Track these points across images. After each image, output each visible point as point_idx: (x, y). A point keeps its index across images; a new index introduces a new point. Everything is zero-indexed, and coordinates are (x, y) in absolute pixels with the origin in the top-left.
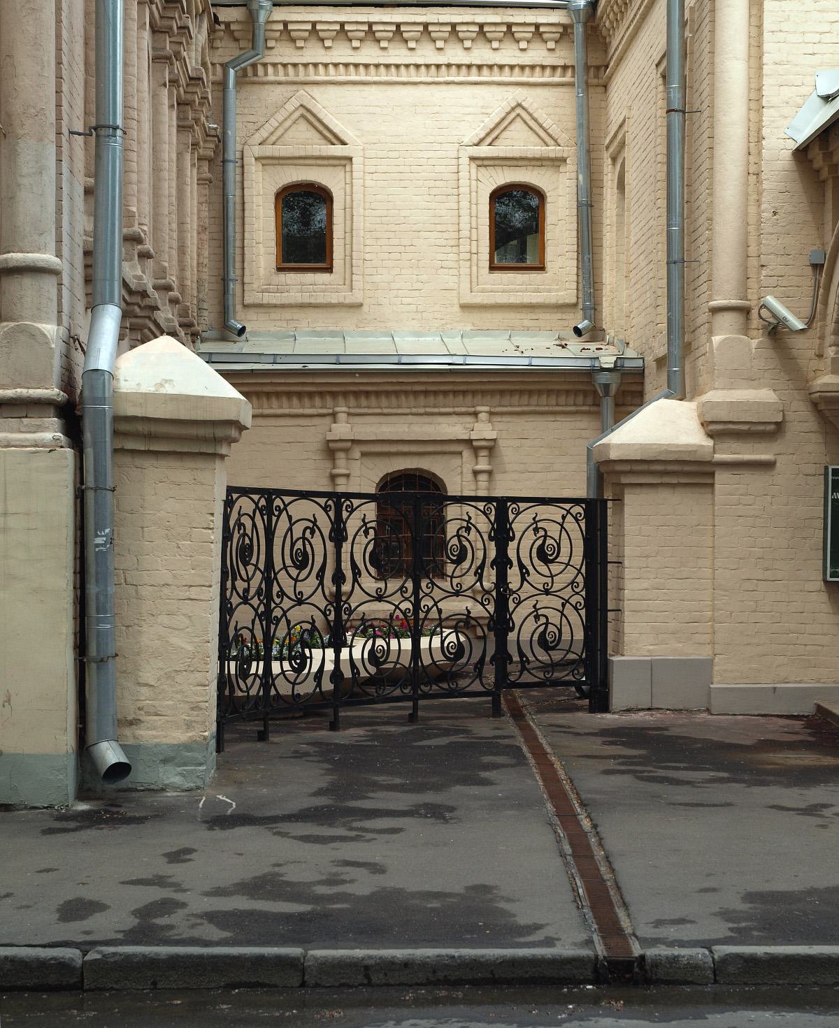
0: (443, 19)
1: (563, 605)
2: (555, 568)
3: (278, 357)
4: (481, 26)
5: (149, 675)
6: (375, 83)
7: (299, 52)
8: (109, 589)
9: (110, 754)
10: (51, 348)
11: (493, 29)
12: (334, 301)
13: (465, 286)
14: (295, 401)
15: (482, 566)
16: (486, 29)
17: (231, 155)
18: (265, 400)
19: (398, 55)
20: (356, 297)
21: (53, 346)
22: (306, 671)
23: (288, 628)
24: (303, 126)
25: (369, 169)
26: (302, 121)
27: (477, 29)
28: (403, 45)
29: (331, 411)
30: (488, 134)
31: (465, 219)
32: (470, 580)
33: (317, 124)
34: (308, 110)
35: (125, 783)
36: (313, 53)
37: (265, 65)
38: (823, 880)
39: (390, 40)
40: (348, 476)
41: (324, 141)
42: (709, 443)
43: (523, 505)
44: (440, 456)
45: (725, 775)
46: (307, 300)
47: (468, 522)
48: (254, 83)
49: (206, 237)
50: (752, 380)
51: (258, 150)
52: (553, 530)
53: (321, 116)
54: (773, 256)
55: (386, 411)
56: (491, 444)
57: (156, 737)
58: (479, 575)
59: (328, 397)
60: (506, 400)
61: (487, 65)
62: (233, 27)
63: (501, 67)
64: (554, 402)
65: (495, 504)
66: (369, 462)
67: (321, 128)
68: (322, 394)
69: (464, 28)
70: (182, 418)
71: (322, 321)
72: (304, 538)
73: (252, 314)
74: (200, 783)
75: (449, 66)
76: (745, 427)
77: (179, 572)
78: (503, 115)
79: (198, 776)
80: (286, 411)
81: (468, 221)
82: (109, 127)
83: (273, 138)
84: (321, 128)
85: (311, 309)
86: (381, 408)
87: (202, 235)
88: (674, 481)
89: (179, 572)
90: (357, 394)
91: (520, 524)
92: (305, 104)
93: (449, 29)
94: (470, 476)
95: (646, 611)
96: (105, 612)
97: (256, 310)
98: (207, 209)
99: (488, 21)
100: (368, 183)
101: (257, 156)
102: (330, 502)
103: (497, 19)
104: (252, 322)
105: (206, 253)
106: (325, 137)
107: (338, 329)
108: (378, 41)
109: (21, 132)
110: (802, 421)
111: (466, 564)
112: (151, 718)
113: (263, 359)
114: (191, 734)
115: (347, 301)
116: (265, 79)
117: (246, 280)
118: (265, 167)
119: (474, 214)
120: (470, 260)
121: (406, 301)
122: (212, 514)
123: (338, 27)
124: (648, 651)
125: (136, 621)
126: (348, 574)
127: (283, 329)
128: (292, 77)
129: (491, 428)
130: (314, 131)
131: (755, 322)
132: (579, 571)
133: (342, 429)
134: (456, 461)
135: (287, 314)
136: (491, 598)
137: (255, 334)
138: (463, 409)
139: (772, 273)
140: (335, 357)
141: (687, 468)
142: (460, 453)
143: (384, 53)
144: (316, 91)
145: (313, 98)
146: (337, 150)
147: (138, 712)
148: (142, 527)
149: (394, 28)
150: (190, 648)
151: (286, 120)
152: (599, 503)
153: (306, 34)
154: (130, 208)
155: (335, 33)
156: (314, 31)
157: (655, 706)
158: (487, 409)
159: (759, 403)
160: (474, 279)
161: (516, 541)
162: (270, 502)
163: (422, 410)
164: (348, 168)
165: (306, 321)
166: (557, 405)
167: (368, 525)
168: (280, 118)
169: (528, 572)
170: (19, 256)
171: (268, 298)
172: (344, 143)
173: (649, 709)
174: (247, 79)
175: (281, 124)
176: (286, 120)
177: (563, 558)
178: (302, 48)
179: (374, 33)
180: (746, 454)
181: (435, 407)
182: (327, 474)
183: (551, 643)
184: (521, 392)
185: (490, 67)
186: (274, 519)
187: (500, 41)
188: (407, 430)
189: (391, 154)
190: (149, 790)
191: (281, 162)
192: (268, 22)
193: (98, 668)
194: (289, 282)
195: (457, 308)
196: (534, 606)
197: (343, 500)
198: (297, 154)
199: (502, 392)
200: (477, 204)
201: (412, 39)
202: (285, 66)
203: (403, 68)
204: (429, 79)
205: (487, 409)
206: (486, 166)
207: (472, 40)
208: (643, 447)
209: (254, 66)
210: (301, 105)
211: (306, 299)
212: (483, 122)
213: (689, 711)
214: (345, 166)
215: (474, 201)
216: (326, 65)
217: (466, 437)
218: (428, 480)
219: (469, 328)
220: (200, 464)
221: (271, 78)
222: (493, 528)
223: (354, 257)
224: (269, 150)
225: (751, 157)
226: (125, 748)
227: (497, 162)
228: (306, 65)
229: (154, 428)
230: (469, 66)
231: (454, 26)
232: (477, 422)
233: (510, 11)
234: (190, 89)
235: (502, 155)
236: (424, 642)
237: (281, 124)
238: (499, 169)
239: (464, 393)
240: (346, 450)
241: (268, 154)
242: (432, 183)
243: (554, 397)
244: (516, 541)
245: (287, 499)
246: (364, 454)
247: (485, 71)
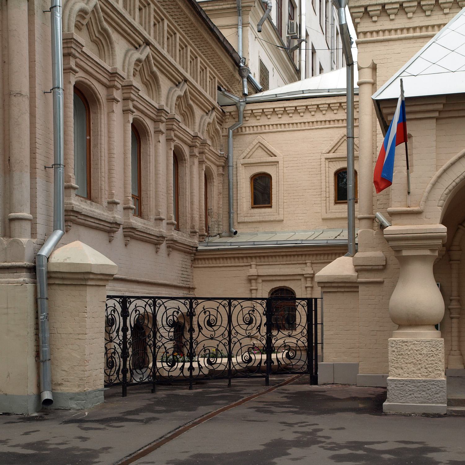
0: (313, 103)
1: (297, 341)
2: (215, 328)
3: (232, 243)
4: (329, 104)
5: (65, 367)
6: (288, 131)
7: (258, 121)
8: (46, 335)
9: (47, 395)
10: (24, 247)
11: (334, 105)
12: (272, 219)
13: (324, 210)
14: (236, 260)
15: (260, 326)
16: (331, 105)
17: (231, 164)
18: (203, 261)
19: (296, 119)
20: (281, 217)
21: (25, 246)
22: (175, 367)
23: (106, 350)
24: (260, 150)
25: (285, 166)
26: (259, 148)
27: (327, 106)
28: (298, 115)
29: (249, 264)
30: (332, 148)
31: (324, 183)
32: (255, 331)
33: (265, 149)
34: (262, 144)
35: (49, 407)
36: (264, 121)
37: (245, 127)
38: (464, 460)
39: (293, 113)
40: (257, 290)
41: (268, 156)
42: (356, 274)
43: (200, 301)
44: (293, 281)
45: (164, 408)
46: (261, 220)
47: (253, 308)
48: (241, 135)
49: (221, 196)
50: (373, 248)
51: (242, 161)
52: (213, 312)
53: (266, 146)
54: (382, 196)
55: (271, 263)
56: (312, 275)
57: (68, 390)
58: (259, 328)
59: (207, 261)
60: (318, 257)
61: (332, 120)
62: (232, 114)
63: (338, 120)
64: (323, 259)
65: (266, 301)
66: (264, 283)
67: (267, 150)
68: (246, 257)
69: (322, 106)
70: (78, 272)
71: (268, 228)
72: (111, 314)
73: (241, 226)
74: (83, 408)
75: (317, 122)
76: (370, 267)
77: (75, 329)
78: (339, 140)
79: (82, 405)
80: (233, 264)
81: (325, 184)
82: (58, 164)
83: (248, 156)
84: (267, 150)
85: (264, 223)
86: (269, 262)
87: (220, 196)
88: (343, 290)
89: (75, 329)
90: (260, 257)
91: (198, 310)
92: (260, 141)
93: (316, 107)
94: (304, 289)
95: (332, 344)
96: (45, 343)
97: (243, 224)
98: (221, 186)
99: (332, 102)
100: (285, 171)
101: (242, 163)
102: (187, 301)
103: (335, 101)
104: (240, 229)
105: (221, 203)
106: (269, 154)
107: (274, 230)
108: (299, 113)
109: (14, 169)
111: (253, 325)
112: (66, 383)
113: (226, 244)
114: (79, 389)
115: (277, 219)
116: (245, 133)
117: (239, 212)
118: (246, 167)
119: (327, 181)
120: (326, 200)
121: (300, 218)
122: (86, 307)
123: (272, 110)
124: (333, 360)
125: (61, 347)
126: (196, 329)
127: (253, 231)
128: (256, 131)
129: (311, 269)
130: (264, 152)
131: (376, 224)
132: (226, 329)
133: (253, 271)
134: (299, 282)
135: (254, 225)
136: (264, 338)
137: (242, 234)
138: (301, 262)
139: (381, 203)
140: (253, 242)
141: (347, 285)
142: (300, 280)
143: (291, 119)
144: (264, 136)
145: (264, 139)
146: (273, 159)
147: (62, 381)
148: (63, 312)
149: (294, 108)
150: (79, 357)
151: (253, 148)
152: (313, 299)
153: (261, 114)
154: (112, 191)
155: (271, 112)
156: (263, 112)
157: (335, 382)
158: (310, 261)
159: (375, 257)
160: (328, 208)
161: (197, 316)
162: (155, 302)
163: (285, 263)
164: (277, 166)
165: (262, 228)
166: (324, 260)
167: (206, 310)
168: (251, 148)
169: (202, 329)
170: (14, 214)
171: (246, 219)
172: (276, 156)
173: (333, 384)
174: (238, 133)
175: (251, 150)
176: (253, 148)
177: (219, 323)
178: (259, 119)
179: (331, 107)
180: (371, 278)
181: (290, 261)
182: (249, 289)
183: (292, 356)
184: (324, 254)
185: (334, 121)
186: (157, 308)
187: (337, 110)
188: (278, 271)
189: (294, 159)
190: (65, 409)
191: (252, 165)
192: (244, 110)
193: (43, 364)
194: (255, 212)
195: (321, 220)
196: (284, 342)
197: (153, 300)
198: (257, 162)
199: (317, 255)
200: (329, 177)
201: (291, 113)
202: (253, 127)
203: (299, 124)
204: (309, 128)
205: (310, 261)
206: (332, 161)
207: (326, 111)
208: (328, 276)
209: (241, 128)
210: (259, 142)
211: (261, 219)
212: (330, 143)
213: (349, 385)
214: (276, 165)
215: (327, 176)
216: (269, 125)
217: (301, 273)
218: (289, 290)
219: (326, 228)
220: (81, 288)
221: (247, 132)
222: (265, 310)
223: (280, 201)
224: (247, 161)
225: (374, 155)
226: (54, 394)
227: (337, 160)
228: (261, 126)
229: (63, 276)
230: (325, 121)
231: (318, 105)
232: (306, 267)
233: (340, 97)
234: (194, 141)
235: (338, 156)
236: (273, 356)
237: (251, 150)
238: (337, 162)
239: (302, 255)
240: (256, 280)
241: (246, 162)
242: (310, 170)
243: (327, 256)
244: (197, 316)
245: (164, 300)
246: (263, 281)
247: (332, 122)
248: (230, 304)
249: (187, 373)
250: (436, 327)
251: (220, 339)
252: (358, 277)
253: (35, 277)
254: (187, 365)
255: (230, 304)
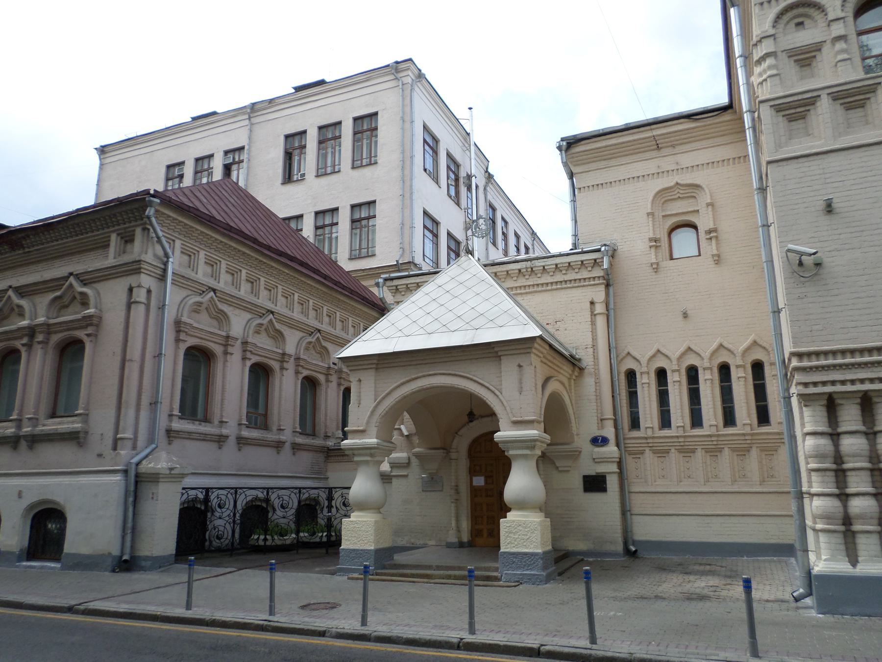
2: (224, 510)
52: (286, 498)
91: (212, 497)
110: (415, 462)
177: (227, 506)
248: (300, 492)
249: (261, 543)
250: (541, 510)
251: (227, 518)
252: (391, 472)
253: (127, 476)
254: (262, 537)
255: (300, 492)
